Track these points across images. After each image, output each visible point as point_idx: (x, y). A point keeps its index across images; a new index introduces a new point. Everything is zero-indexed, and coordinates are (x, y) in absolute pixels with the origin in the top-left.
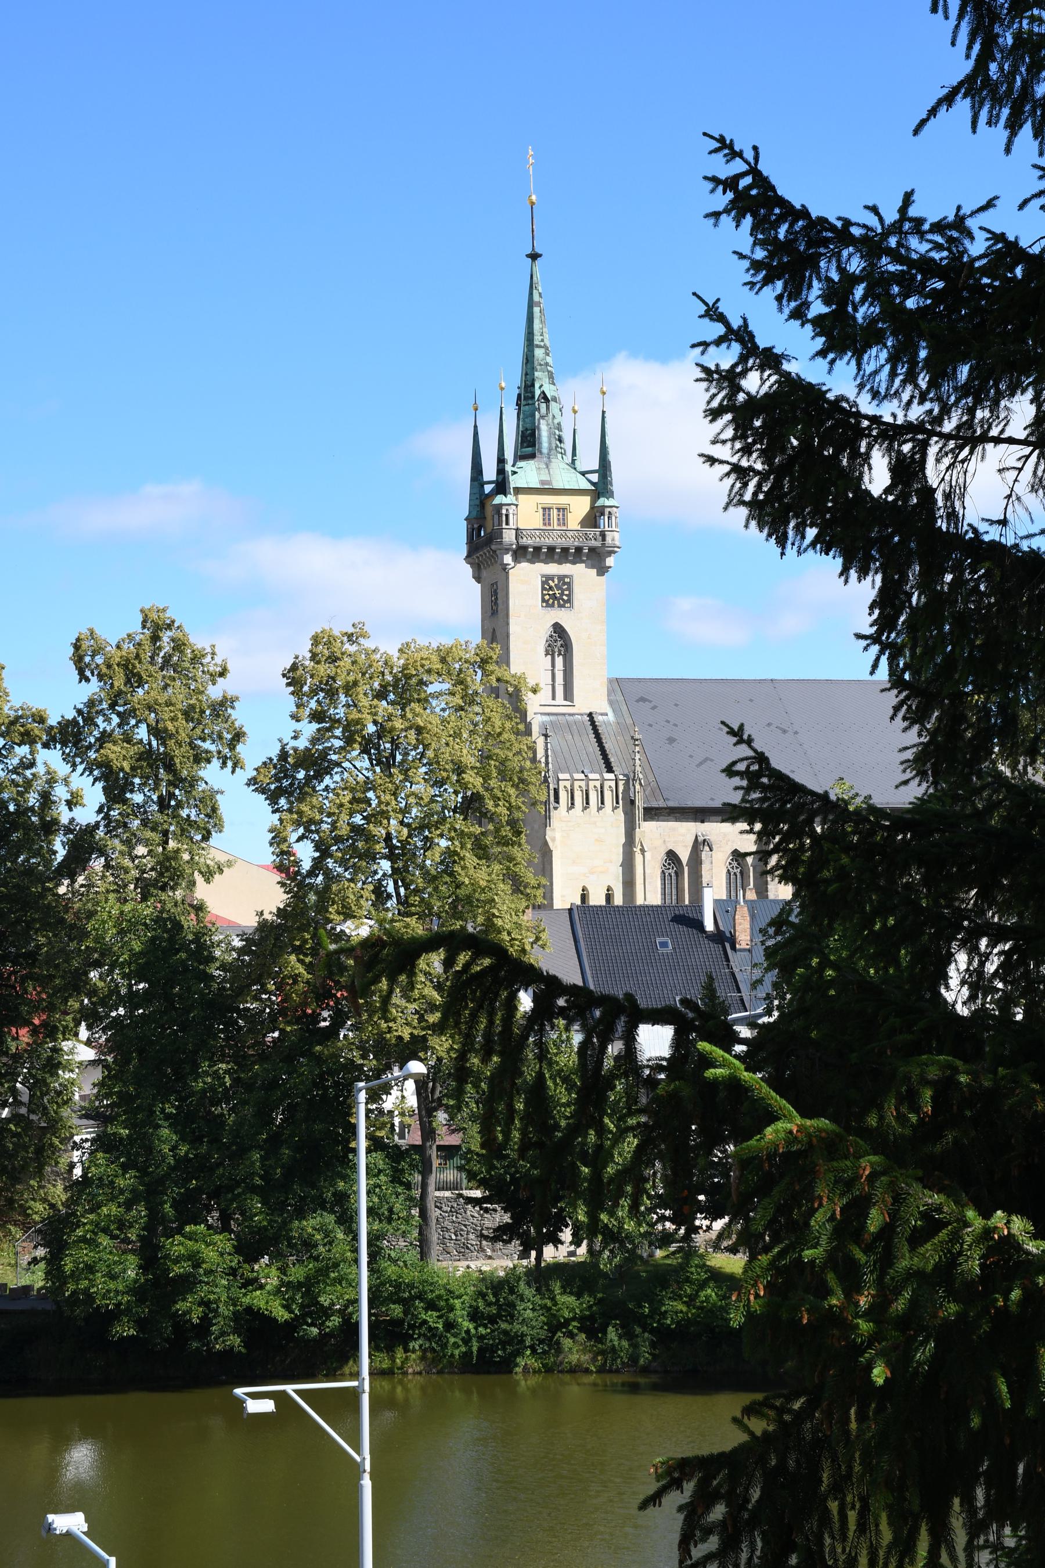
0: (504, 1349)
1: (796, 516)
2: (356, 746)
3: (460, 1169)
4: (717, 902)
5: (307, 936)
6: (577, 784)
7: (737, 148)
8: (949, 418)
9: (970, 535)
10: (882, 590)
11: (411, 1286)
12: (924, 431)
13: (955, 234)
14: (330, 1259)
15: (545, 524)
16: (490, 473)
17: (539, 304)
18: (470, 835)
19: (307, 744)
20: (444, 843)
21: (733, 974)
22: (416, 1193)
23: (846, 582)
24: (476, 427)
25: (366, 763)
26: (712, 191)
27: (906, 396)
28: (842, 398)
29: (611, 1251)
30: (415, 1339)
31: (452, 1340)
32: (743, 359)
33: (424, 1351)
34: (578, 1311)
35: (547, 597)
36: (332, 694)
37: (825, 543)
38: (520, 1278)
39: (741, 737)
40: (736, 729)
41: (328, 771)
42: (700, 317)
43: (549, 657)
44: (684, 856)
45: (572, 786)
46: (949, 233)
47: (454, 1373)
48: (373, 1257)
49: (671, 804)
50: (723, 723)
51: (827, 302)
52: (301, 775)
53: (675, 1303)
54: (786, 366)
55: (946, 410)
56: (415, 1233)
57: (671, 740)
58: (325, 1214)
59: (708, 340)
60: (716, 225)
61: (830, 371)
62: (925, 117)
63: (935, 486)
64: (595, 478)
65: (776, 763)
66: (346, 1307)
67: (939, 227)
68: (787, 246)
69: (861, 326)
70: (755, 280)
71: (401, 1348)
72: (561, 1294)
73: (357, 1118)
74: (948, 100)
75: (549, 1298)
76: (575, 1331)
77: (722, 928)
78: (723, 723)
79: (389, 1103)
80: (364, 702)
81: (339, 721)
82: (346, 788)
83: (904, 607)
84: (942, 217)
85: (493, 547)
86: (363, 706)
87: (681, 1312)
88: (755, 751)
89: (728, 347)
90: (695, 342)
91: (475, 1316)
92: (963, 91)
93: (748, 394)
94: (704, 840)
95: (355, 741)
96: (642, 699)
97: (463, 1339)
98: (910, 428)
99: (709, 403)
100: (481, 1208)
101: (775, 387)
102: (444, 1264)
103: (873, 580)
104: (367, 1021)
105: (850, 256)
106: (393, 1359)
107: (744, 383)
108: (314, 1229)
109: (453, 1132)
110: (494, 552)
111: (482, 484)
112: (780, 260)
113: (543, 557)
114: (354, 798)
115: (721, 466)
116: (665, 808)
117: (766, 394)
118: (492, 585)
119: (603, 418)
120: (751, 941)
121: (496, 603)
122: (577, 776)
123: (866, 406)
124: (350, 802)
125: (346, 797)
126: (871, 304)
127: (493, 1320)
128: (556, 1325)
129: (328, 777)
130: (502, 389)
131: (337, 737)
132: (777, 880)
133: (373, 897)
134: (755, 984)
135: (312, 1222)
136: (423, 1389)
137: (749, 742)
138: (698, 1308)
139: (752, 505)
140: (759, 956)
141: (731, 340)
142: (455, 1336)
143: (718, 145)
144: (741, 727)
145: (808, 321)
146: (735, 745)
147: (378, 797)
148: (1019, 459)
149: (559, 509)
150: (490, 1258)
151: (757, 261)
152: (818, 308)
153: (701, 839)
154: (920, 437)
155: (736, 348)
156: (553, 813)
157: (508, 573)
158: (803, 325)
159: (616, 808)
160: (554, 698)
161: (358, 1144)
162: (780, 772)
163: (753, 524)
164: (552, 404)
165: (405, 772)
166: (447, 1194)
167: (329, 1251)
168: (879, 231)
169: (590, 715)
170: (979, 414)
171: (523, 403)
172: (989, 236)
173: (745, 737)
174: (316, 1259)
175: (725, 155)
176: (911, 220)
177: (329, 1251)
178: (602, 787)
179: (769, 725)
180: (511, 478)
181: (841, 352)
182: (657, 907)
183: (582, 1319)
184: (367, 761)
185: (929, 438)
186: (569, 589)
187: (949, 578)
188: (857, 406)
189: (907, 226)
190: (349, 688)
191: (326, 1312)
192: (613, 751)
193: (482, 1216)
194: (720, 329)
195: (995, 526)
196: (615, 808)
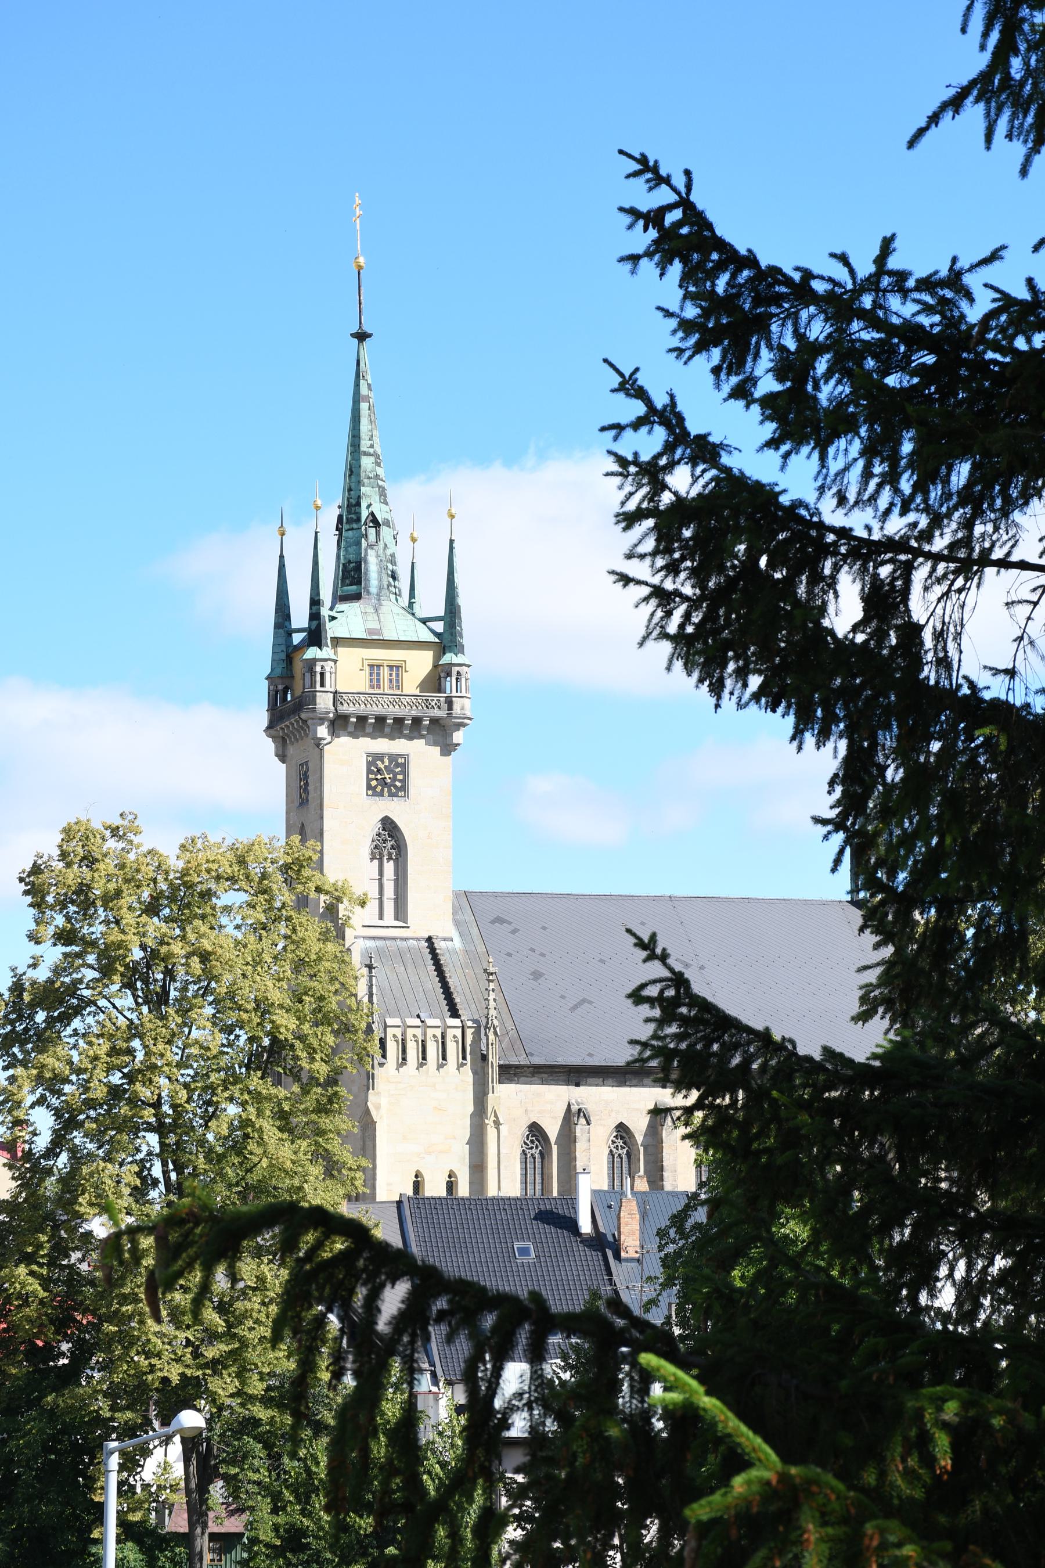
1: (736, 658)
2: (117, 978)
4: (595, 1193)
5: (43, 1238)
6: (410, 1032)
7: (663, 172)
8: (941, 535)
9: (965, 690)
10: (847, 761)
12: (909, 550)
13: (949, 294)
15: (372, 687)
16: (300, 618)
17: (367, 399)
18: (269, 1098)
23: (800, 748)
24: (282, 557)
26: (630, 227)
27: (883, 502)
28: (799, 503)
32: (669, 448)
36: (86, 906)
39: (653, 951)
40: (646, 940)
41: (78, 1011)
42: (613, 391)
43: (376, 862)
44: (553, 1131)
45: (404, 1034)
46: (941, 293)
49: (537, 1060)
51: (780, 378)
52: (40, 1017)
54: (725, 460)
55: (937, 522)
57: (537, 975)
59: (623, 422)
60: (633, 272)
61: (783, 468)
62: (923, 124)
63: (922, 622)
64: (439, 627)
65: (698, 988)
67: (927, 284)
70: (682, 345)
74: (956, 103)
77: (602, 1230)
79: (149, 1471)
81: (93, 944)
82: (102, 1035)
83: (876, 783)
84: (932, 271)
85: (303, 716)
89: (650, 432)
92: (975, 92)
93: (675, 493)
94: (580, 1110)
96: (499, 920)
98: (891, 545)
99: (623, 503)
101: (710, 487)
104: (120, 1358)
105: (811, 318)
107: (669, 479)
109: (232, 1513)
110: (305, 722)
111: (289, 634)
112: (717, 321)
113: (369, 730)
115: (637, 587)
116: (528, 1067)
117: (699, 495)
118: (302, 765)
119: (451, 549)
120: (642, 1247)
121: (306, 790)
123: (832, 516)
125: (103, 1047)
126: (839, 382)
130: (318, 508)
139: (679, 639)
140: (655, 1268)
141: (654, 422)
143: (638, 167)
145: (754, 401)
146: (645, 961)
147: (145, 1047)
148: (1034, 590)
149: (391, 667)
152: (768, 385)
154: (903, 557)
155: (660, 435)
156: (378, 1072)
157: (322, 750)
158: (747, 407)
159: (463, 1065)
160: (381, 917)
162: (704, 999)
163: (678, 665)
164: (384, 529)
165: (183, 1012)
168: (850, 286)
169: (429, 940)
170: (978, 529)
171: (345, 526)
172: (997, 296)
175: (648, 181)
176: (891, 273)
178: (443, 1037)
180: (329, 625)
181: (799, 442)
182: (516, 1199)
184: (131, 999)
185: (915, 559)
187: (936, 746)
188: (820, 514)
189: (886, 281)
190: (110, 899)
192: (459, 989)
194: (639, 408)
195: (1001, 677)
196: (460, 1066)
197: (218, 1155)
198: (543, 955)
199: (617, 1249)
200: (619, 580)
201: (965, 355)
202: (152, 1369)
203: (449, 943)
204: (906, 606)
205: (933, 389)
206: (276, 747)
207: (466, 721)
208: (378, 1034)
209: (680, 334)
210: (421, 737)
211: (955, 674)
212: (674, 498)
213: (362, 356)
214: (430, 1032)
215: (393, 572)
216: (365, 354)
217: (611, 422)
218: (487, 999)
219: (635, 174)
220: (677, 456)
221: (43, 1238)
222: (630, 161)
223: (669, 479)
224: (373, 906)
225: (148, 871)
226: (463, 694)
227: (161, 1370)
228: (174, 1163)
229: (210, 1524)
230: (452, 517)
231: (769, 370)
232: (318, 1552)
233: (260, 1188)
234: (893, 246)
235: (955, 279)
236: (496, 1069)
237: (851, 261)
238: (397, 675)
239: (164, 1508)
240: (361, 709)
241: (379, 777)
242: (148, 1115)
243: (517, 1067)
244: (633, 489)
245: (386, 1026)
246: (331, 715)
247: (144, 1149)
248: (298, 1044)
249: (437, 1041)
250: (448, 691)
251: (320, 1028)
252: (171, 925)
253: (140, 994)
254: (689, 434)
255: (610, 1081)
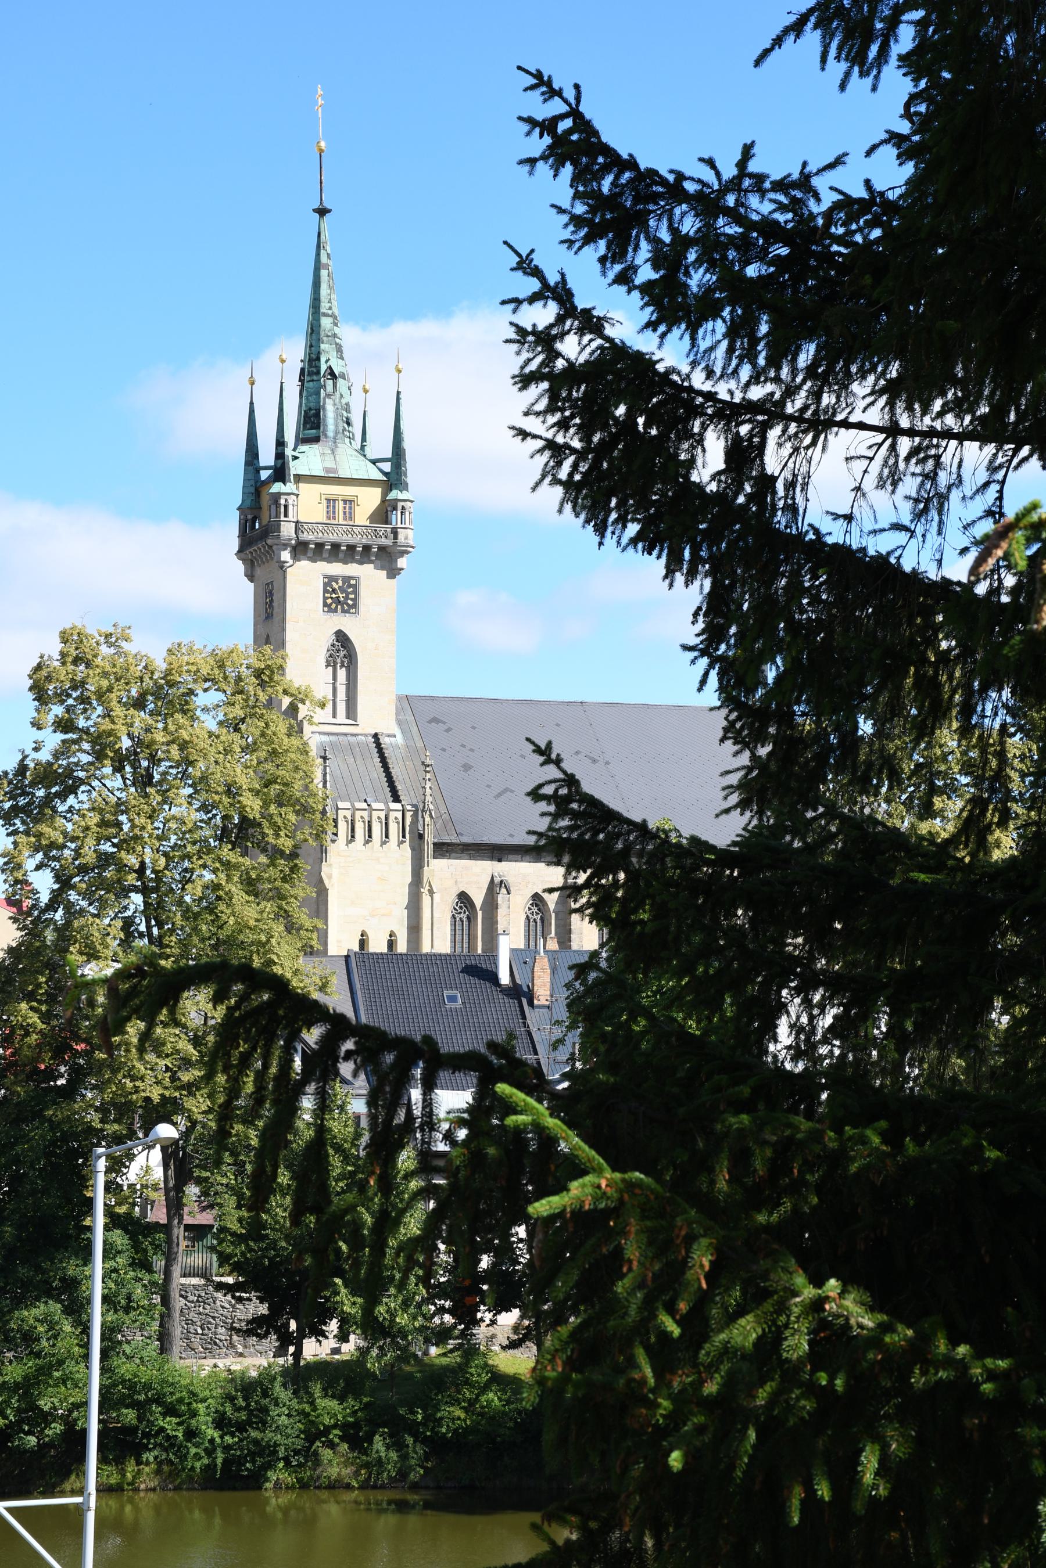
0: (253, 1462)
3: (212, 1249)
4: (513, 951)
6: (358, 814)
9: (811, 536)
11: (147, 1387)
13: (798, 194)
14: (54, 1355)
15: (328, 518)
16: (267, 457)
17: (327, 267)
18: (237, 866)
19: (50, 758)
20: (208, 876)
21: (529, 1034)
22: (159, 1278)
23: (671, 586)
24: (252, 403)
25: (118, 782)
26: (528, 134)
29: (381, 1348)
30: (150, 1450)
31: (193, 1450)
32: (560, 320)
33: (160, 1464)
34: (340, 1417)
35: (329, 601)
37: (647, 541)
38: (275, 1378)
39: (549, 756)
40: (543, 747)
41: (73, 790)
42: (512, 269)
43: (330, 669)
44: (478, 899)
45: (353, 815)
46: (793, 193)
47: (193, 1489)
48: (105, 1355)
49: (465, 839)
50: (528, 740)
51: (656, 268)
53: (452, 1409)
54: (609, 331)
55: (790, 392)
56: (155, 1326)
57: (467, 767)
58: (51, 1302)
59: (521, 297)
60: (531, 173)
63: (776, 474)
64: (387, 467)
65: (587, 787)
66: (70, 1411)
67: (781, 185)
68: (611, 202)
69: (695, 296)
71: (133, 1462)
72: (322, 1397)
73: (94, 1191)
75: (308, 1402)
76: (337, 1440)
77: (518, 981)
78: (528, 740)
79: (133, 1173)
80: (118, 711)
84: (785, 174)
85: (269, 542)
86: (117, 716)
87: (459, 1418)
88: (565, 772)
89: (545, 305)
90: (506, 298)
91: (221, 1422)
94: (501, 882)
95: (106, 756)
96: (435, 720)
97: (206, 1450)
98: (750, 407)
99: (522, 368)
100: (233, 1297)
101: (596, 354)
102: (188, 1362)
103: (702, 585)
105: (683, 214)
106: (122, 1473)
107: (559, 346)
108: (37, 1320)
109: (203, 1209)
110: (270, 547)
111: (258, 470)
112: (603, 215)
113: (325, 555)
114: (102, 820)
115: (534, 441)
116: (458, 844)
117: (587, 362)
119: (398, 399)
120: (552, 996)
121: (271, 606)
122: (358, 805)
123: (699, 381)
124: (98, 825)
125: (93, 819)
126: (706, 271)
127: (241, 1427)
128: (314, 1433)
129: (72, 797)
131: (84, 751)
132: (587, 919)
133: (122, 935)
134: (556, 1045)
135: (34, 1312)
136: (157, 1509)
137: (558, 762)
138: (479, 1414)
139: (568, 485)
140: (562, 1013)
141: (547, 298)
142: (197, 1445)
143: (534, 81)
144: (549, 744)
145: (635, 287)
146: (542, 765)
147: (131, 820)
148: (870, 447)
149: (345, 501)
150: (241, 1355)
151: (579, 216)
152: (646, 274)
153: (497, 880)
154: (760, 418)
156: (332, 849)
157: (285, 572)
158: (629, 292)
159: (402, 842)
160: (334, 716)
161: (93, 1221)
162: (592, 797)
163: (568, 507)
164: (340, 381)
166: (195, 1281)
167: (54, 1345)
168: (716, 187)
171: (307, 378)
173: (554, 756)
174: (38, 1355)
175: (543, 94)
176: (751, 176)
177: (54, 1345)
178: (387, 818)
179: (577, 753)
180: (292, 464)
182: (446, 955)
183: (345, 1426)
186: (355, 592)
189: (747, 183)
190: (100, 695)
191: (46, 1418)
192: (400, 778)
193: (233, 1306)
194: (534, 285)
196: (400, 843)
197: (194, 914)
198: (472, 750)
199: (531, 998)
200: (517, 435)
201: (814, 247)
202: (137, 1090)
203: (392, 739)
204: (762, 460)
205: (787, 277)
206: (246, 568)
207: (409, 549)
208: (330, 814)
209: (571, 228)
210: (371, 562)
211: (800, 519)
212: (566, 364)
213: (322, 230)
214: (375, 814)
215: (347, 418)
216: (325, 226)
217: (511, 296)
218: (424, 788)
219: (532, 88)
220: (567, 328)
221: (42, 979)
222: (527, 76)
223: (559, 346)
224: (329, 706)
225: (137, 670)
226: (407, 526)
227: (144, 1091)
228: (156, 919)
229: (185, 1217)
230: (399, 371)
231: (647, 260)
232: (275, 1242)
233: (230, 942)
234: (753, 152)
235: (804, 182)
236: (431, 846)
237: (717, 164)
238: (350, 508)
239: (147, 1202)
240: (319, 537)
241: (334, 596)
242: (131, 879)
243: (449, 844)
244: (531, 355)
245: (338, 809)
246: (293, 542)
247: (132, 907)
248: (265, 824)
249: (381, 822)
250: (394, 523)
251: (284, 809)
252: (155, 718)
253: (128, 776)
254: (576, 308)
255: (528, 858)
